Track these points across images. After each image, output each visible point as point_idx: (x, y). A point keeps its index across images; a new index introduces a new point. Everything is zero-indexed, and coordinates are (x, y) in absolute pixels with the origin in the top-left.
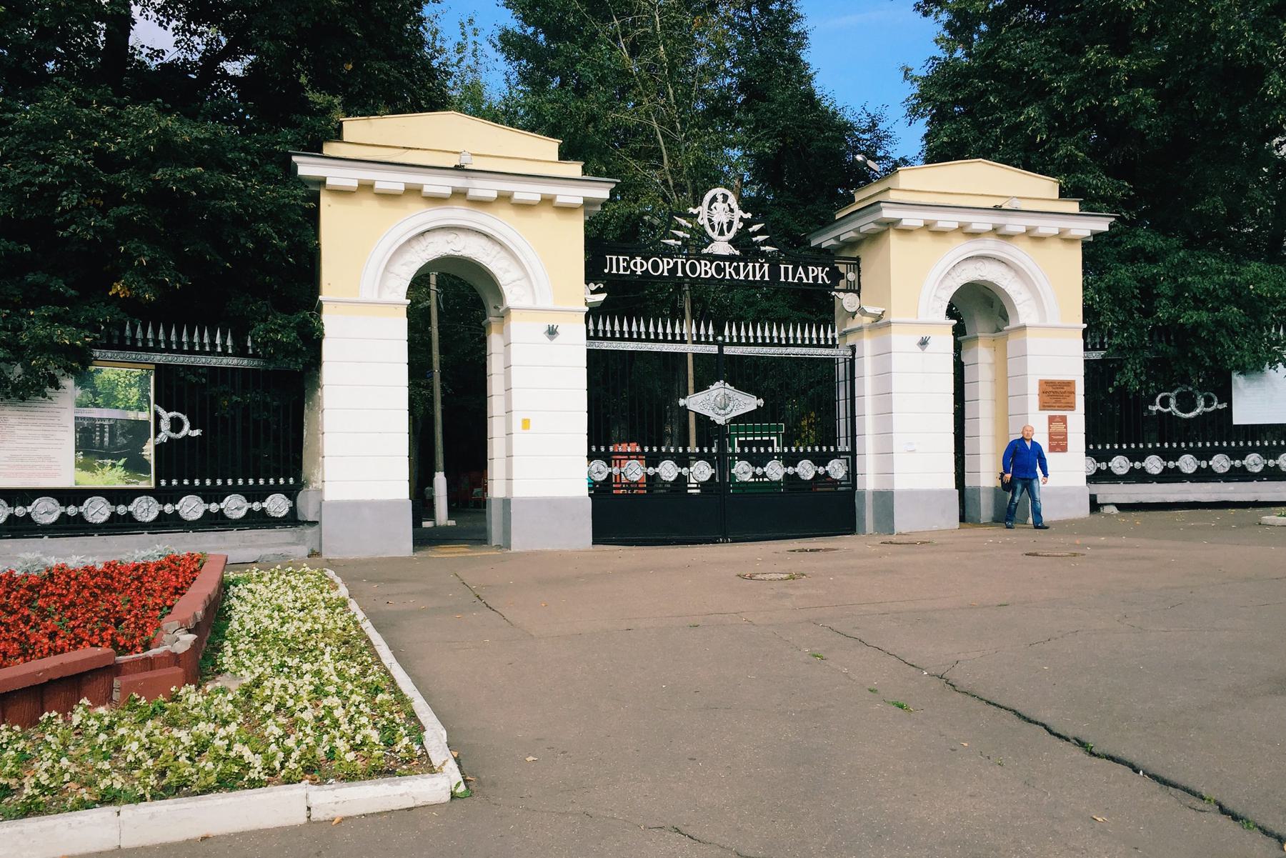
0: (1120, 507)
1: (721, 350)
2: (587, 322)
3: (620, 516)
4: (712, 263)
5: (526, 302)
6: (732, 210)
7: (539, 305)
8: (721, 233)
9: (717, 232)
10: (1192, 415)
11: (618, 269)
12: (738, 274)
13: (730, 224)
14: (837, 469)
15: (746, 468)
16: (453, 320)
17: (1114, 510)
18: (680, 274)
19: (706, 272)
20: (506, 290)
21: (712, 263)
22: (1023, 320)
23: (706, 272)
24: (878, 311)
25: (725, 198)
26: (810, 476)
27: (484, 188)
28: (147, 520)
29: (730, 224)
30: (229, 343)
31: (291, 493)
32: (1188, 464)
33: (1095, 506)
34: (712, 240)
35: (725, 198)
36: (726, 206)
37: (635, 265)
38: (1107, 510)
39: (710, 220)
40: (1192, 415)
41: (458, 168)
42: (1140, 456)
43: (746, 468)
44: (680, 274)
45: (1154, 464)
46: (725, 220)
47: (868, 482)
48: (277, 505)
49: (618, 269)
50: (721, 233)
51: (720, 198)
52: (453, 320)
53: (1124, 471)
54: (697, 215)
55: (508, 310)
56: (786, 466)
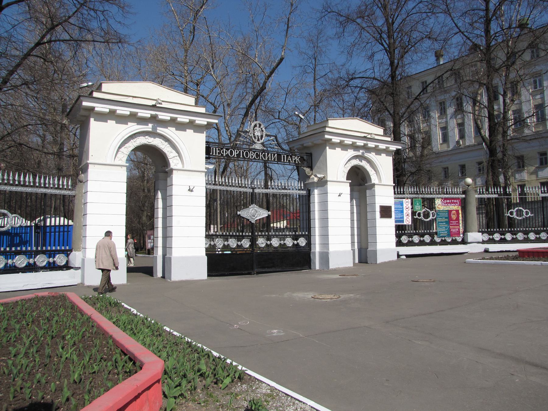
0: (407, 256)
1: (253, 191)
2: (394, 189)
3: (220, 264)
4: (254, 152)
5: (180, 166)
6: (262, 131)
7: (185, 168)
8: (258, 140)
9: (256, 140)
10: (428, 220)
11: (216, 153)
12: (265, 158)
13: (262, 136)
14: (302, 242)
15: (263, 242)
16: (149, 175)
17: (404, 257)
18: (241, 157)
19: (252, 156)
20: (171, 161)
21: (254, 152)
22: (373, 182)
23: (252, 156)
24: (322, 176)
25: (260, 125)
26: (235, 246)
27: (164, 116)
28: (62, 264)
29: (262, 136)
30: (70, 184)
31: (67, 252)
32: (520, 236)
33: (399, 256)
34: (255, 143)
35: (260, 125)
36: (260, 129)
37: (223, 151)
38: (402, 257)
39: (254, 134)
40: (428, 220)
41: (154, 106)
42: (503, 233)
43: (263, 242)
44: (241, 157)
45: (508, 237)
46: (259, 134)
47: (317, 248)
48: (60, 259)
49: (216, 153)
50: (258, 140)
51: (258, 125)
52: (149, 175)
53: (406, 242)
54: (249, 132)
55: (172, 170)
56: (238, 241)
